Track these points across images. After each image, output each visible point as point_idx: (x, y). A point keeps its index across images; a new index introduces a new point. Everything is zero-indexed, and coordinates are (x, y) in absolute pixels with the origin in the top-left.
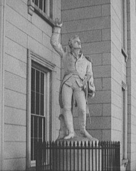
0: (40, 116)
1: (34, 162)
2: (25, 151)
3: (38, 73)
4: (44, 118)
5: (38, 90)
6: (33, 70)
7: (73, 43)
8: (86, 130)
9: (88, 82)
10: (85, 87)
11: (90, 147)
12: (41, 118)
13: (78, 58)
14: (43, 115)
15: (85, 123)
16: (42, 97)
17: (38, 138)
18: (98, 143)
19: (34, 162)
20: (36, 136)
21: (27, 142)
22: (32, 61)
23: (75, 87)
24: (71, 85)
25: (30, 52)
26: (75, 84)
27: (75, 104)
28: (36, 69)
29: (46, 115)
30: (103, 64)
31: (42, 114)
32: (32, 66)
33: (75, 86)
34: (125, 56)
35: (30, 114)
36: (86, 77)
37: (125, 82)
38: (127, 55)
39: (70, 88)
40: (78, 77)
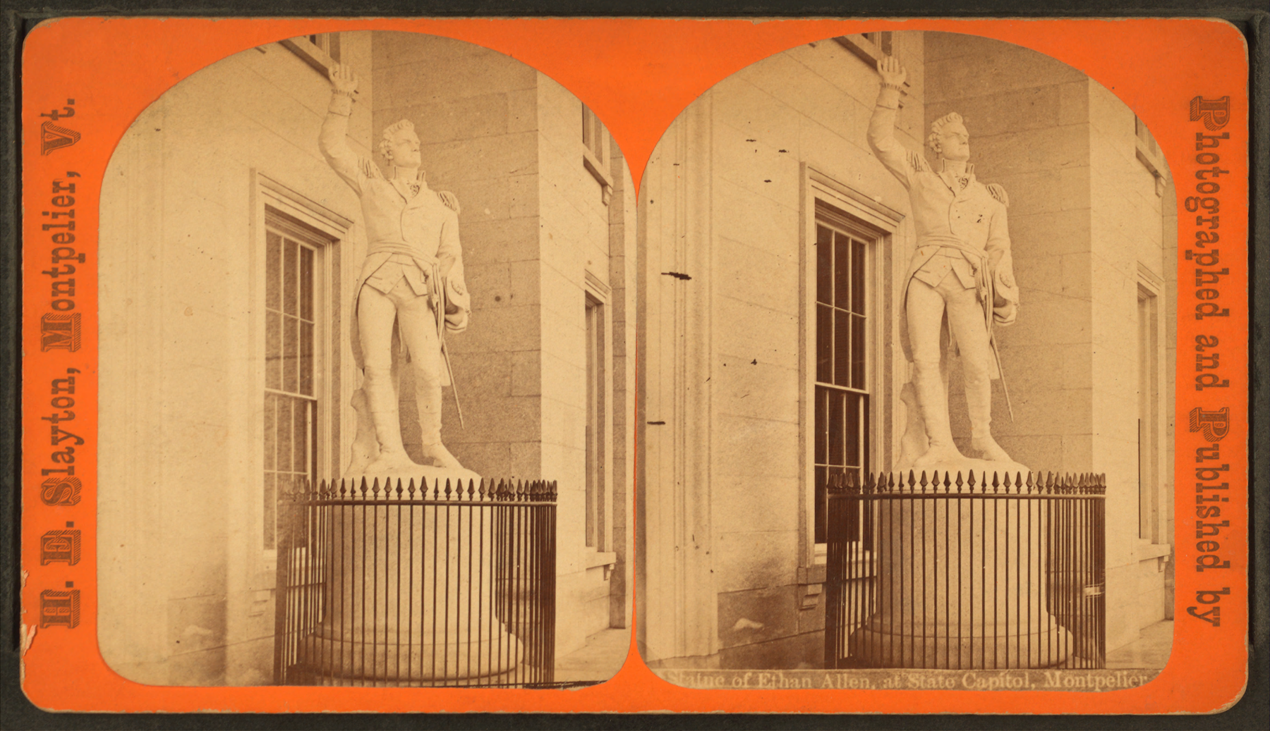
0: (850, 389)
1: (823, 548)
2: (795, 512)
5: (841, 301)
6: (822, 233)
7: (941, 140)
8: (448, 446)
9: (993, 274)
11: (997, 492)
12: (857, 396)
13: (957, 191)
16: (859, 325)
17: (845, 466)
18: (477, 486)
19: (823, 548)
20: (836, 459)
21: (801, 478)
22: (818, 202)
24: (386, 288)
25: (808, 173)
27: (401, 355)
28: (851, 236)
29: (873, 384)
30: (513, 215)
31: (859, 382)
32: (817, 216)
33: (951, 286)
34: (603, 184)
35: (811, 381)
36: (437, 261)
37: (602, 276)
38: (609, 180)
40: (957, 253)
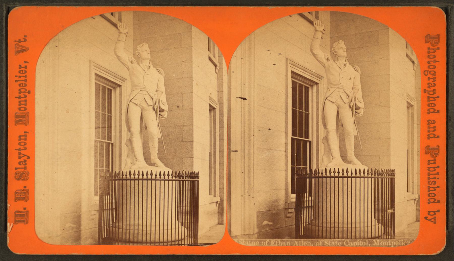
0: (304, 139)
1: (294, 196)
3: (301, 86)
4: (310, 142)
5: (301, 108)
6: (294, 83)
7: (337, 50)
8: (160, 159)
9: (355, 98)
10: (352, 105)
11: (356, 175)
12: (306, 141)
14: (308, 138)
15: (353, 147)
16: (307, 116)
17: (302, 166)
18: (170, 174)
19: (294, 196)
20: (299, 164)
21: (286, 171)
22: (293, 72)
23: (143, 105)
24: (138, 103)
26: (340, 100)
27: (144, 127)
29: (312, 137)
31: (307, 136)
32: (292, 77)
33: (340, 102)
34: (216, 66)
35: (290, 136)
37: (215, 98)
38: (218, 64)
39: (334, 105)
40: (342, 90)
